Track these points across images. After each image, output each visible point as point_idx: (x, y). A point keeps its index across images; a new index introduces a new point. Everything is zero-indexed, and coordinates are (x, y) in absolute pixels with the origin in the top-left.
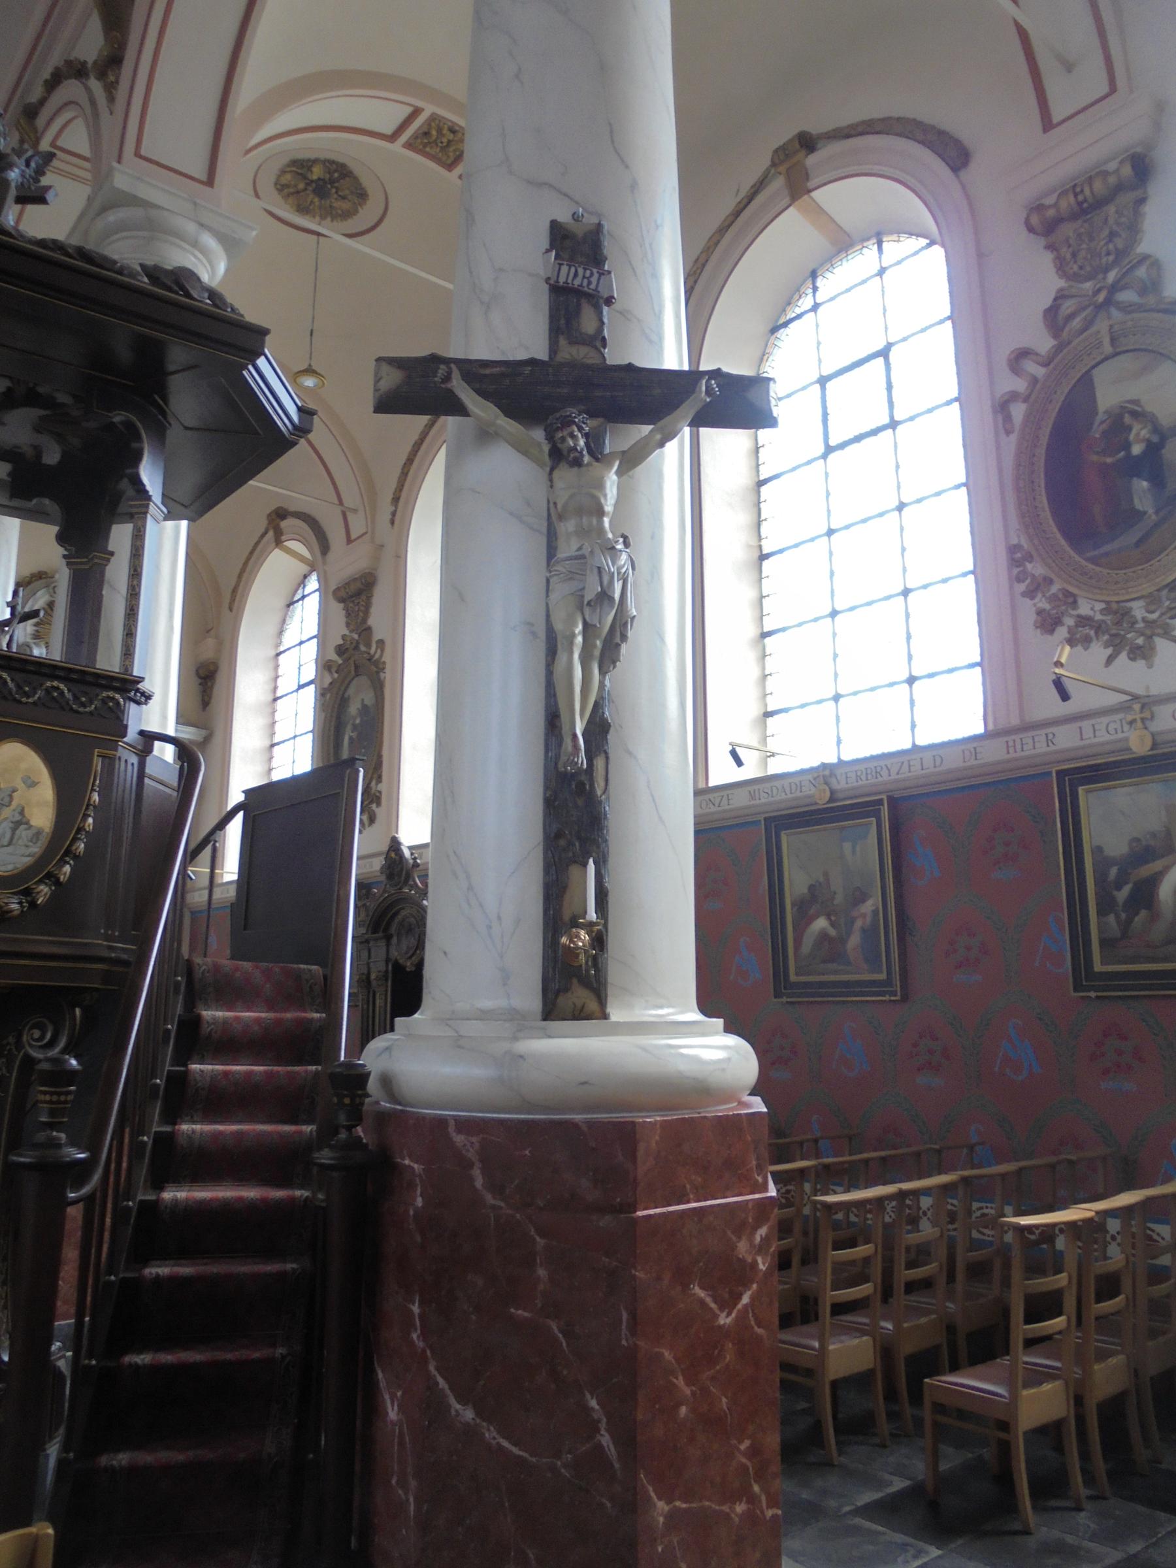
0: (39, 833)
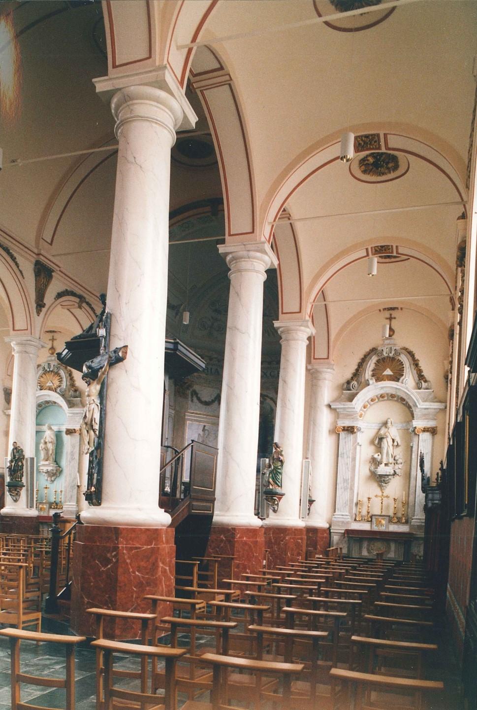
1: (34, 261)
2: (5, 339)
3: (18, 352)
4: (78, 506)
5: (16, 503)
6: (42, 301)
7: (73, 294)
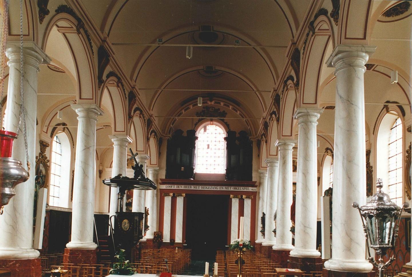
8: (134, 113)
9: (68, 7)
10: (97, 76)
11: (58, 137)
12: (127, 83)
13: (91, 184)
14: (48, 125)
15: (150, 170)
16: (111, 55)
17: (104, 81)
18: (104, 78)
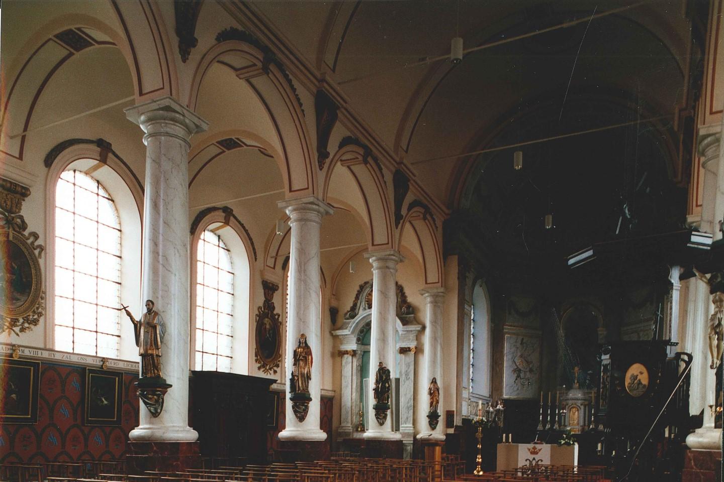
0: (645, 385)
1: (394, 170)
2: (365, 255)
3: (296, 221)
4: (414, 428)
5: (301, 423)
6: (325, 147)
7: (256, 43)
8: (409, 209)
9: (247, 33)
10: (393, 212)
11: (221, 237)
12: (298, 67)
13: (392, 355)
14: (275, 255)
15: (428, 296)
16: (341, 106)
17: (403, 216)
18: (404, 212)
